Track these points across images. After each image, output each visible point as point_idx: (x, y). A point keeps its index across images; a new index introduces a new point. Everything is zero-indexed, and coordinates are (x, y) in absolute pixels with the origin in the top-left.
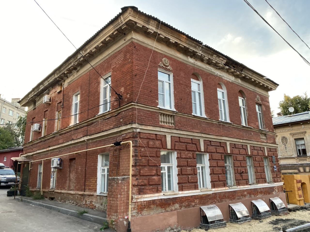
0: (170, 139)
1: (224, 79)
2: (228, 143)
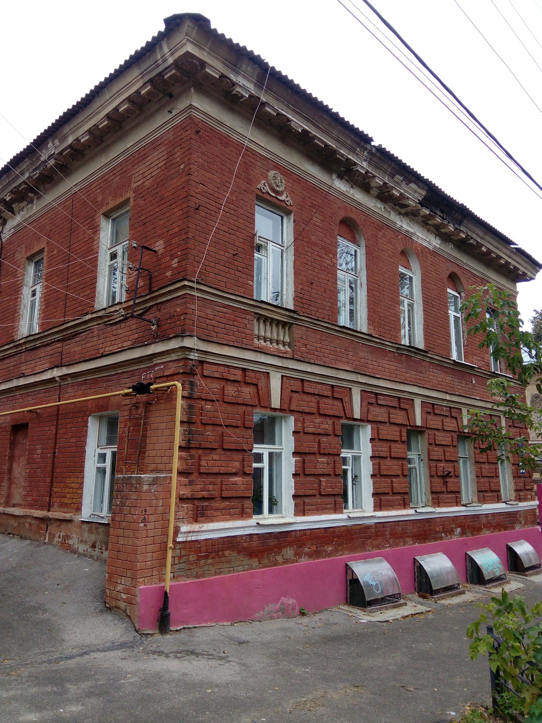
1: (417, 242)
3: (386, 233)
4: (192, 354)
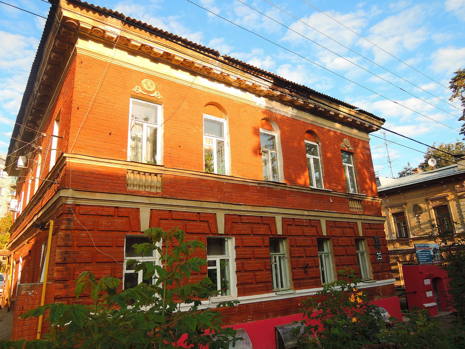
0: (148, 215)
1: (276, 113)
2: (359, 223)
3: (247, 109)
4: (68, 200)
